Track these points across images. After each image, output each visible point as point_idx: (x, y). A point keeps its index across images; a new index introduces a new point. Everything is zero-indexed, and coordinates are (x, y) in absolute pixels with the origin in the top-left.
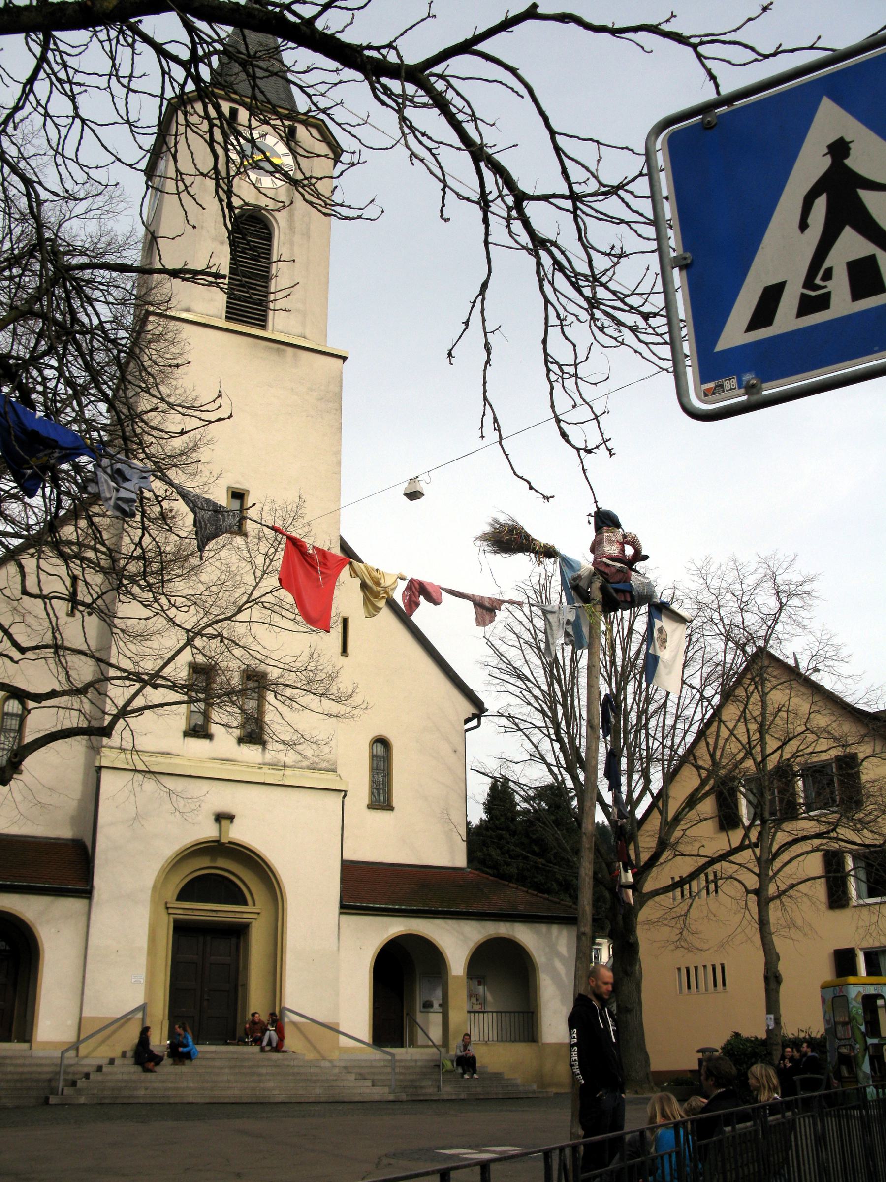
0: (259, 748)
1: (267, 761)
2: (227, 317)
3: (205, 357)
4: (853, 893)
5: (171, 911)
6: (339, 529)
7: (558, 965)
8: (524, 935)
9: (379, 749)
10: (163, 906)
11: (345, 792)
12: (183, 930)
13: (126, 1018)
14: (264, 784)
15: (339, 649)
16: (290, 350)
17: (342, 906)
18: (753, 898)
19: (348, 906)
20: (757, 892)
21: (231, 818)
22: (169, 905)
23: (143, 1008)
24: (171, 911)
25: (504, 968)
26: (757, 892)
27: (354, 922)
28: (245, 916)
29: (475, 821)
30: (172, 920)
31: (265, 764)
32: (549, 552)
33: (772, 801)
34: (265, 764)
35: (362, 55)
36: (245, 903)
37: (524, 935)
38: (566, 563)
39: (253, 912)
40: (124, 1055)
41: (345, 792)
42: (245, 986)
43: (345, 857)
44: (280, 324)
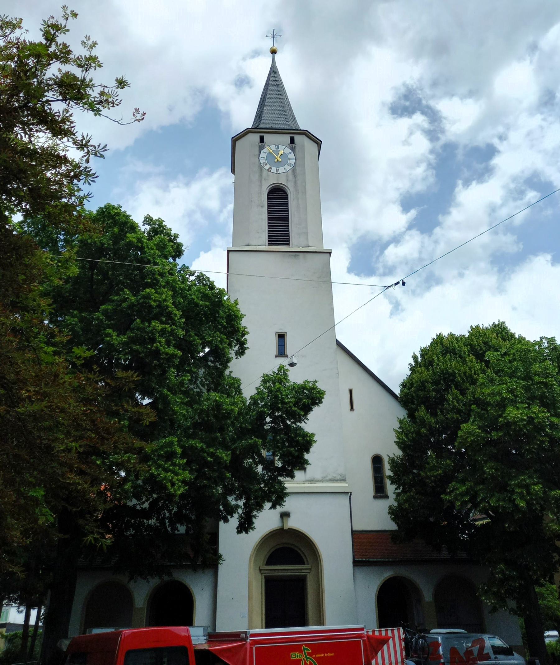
0: (303, 471)
1: (307, 479)
2: (269, 244)
5: (262, 572)
6: (333, 328)
10: (258, 569)
11: (351, 493)
14: (305, 493)
15: (289, 340)
16: (301, 254)
17: (356, 563)
19: (358, 563)
22: (261, 568)
24: (262, 572)
27: (362, 572)
28: (303, 571)
29: (50, 135)
30: (263, 577)
31: (307, 481)
34: (307, 481)
35: (372, 659)
36: (302, 563)
41: (351, 493)
43: (354, 529)
44: (296, 242)
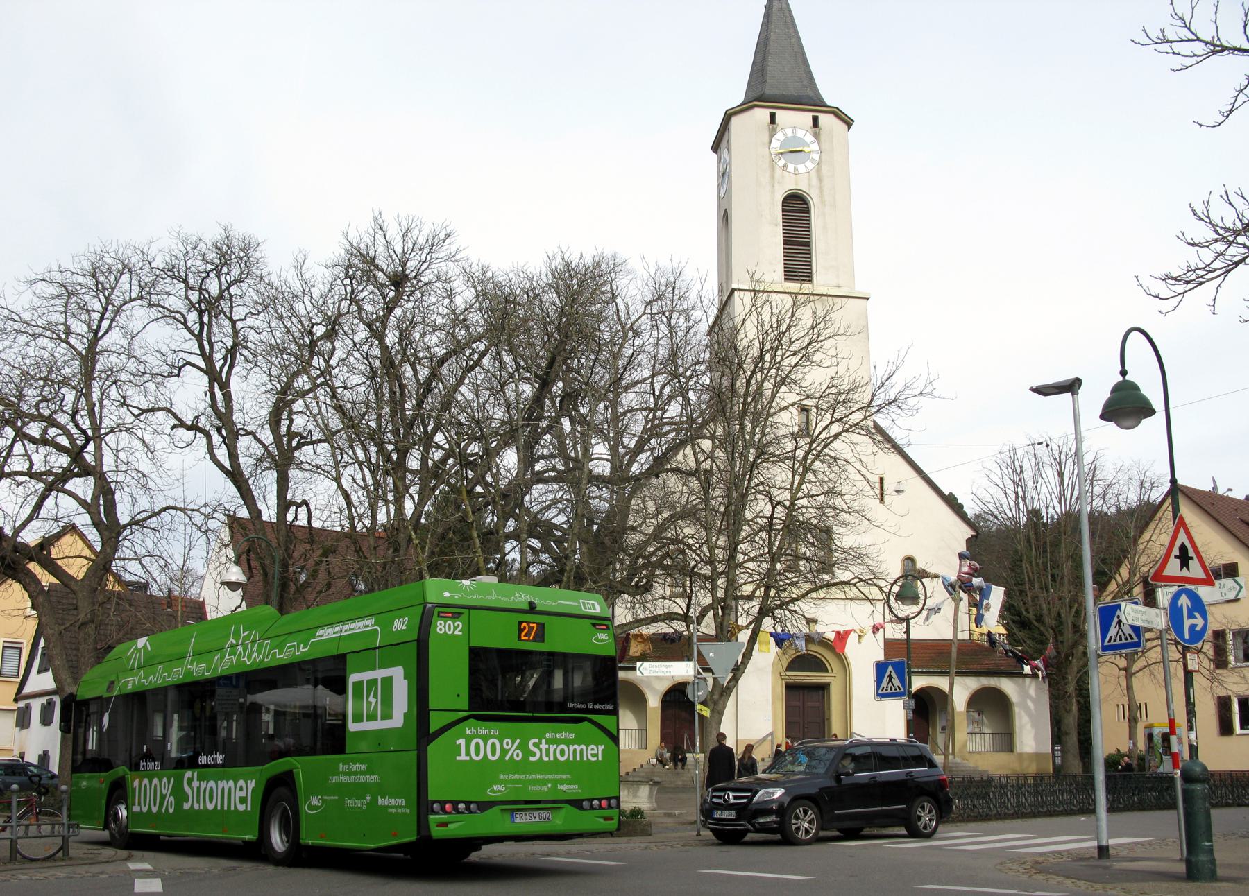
3: (819, 628)
4: (1231, 658)
7: (1030, 704)
8: (1007, 686)
9: (909, 562)
12: (790, 688)
13: (763, 740)
18: (1123, 672)
20: (1125, 669)
21: (816, 621)
23: (771, 734)
25: (991, 705)
26: (1125, 669)
32: (936, 576)
33: (794, 773)
37: (1007, 686)
38: (944, 579)
39: (832, 676)
40: (661, 761)
42: (829, 720)
